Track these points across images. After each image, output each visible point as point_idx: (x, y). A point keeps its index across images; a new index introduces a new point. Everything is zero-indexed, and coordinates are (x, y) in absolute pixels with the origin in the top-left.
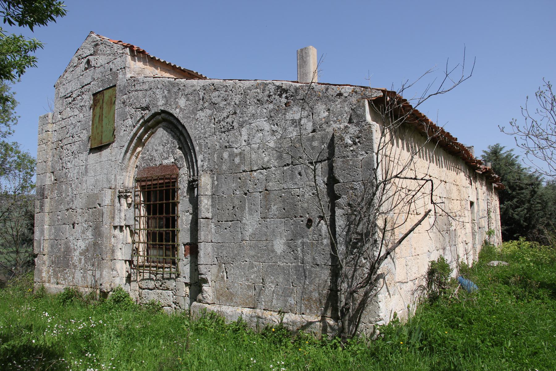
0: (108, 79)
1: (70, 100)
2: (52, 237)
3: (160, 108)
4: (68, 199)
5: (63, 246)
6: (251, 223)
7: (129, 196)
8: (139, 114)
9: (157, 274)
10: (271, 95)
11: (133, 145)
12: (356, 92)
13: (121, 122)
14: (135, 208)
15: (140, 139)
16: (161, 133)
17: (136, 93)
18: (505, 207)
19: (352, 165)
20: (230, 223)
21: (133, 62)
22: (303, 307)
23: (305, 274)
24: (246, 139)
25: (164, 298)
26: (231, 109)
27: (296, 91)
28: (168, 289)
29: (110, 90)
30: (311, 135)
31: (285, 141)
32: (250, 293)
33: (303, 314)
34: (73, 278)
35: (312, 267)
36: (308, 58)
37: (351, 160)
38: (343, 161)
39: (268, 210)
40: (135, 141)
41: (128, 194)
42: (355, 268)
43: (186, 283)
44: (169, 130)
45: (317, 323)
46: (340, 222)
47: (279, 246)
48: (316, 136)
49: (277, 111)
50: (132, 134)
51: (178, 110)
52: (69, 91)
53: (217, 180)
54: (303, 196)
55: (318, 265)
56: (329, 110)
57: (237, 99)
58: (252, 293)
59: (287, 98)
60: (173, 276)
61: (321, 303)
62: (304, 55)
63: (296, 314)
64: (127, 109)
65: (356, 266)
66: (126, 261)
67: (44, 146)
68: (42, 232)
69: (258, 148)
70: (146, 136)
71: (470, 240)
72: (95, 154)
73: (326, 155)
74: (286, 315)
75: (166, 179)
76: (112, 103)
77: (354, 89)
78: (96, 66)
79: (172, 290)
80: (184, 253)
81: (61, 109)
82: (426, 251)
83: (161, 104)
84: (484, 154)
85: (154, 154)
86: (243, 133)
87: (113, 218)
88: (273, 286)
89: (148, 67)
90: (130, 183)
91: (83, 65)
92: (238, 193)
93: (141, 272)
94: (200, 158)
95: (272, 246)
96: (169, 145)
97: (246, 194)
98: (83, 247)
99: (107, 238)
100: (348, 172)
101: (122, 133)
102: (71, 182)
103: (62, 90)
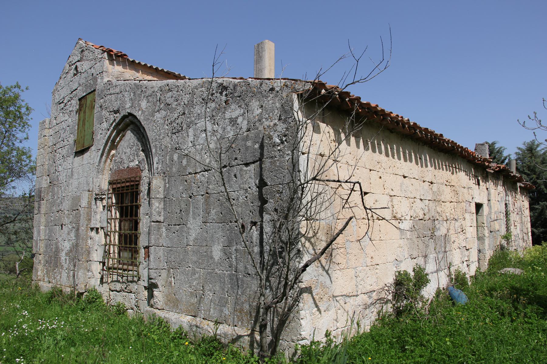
0: (90, 83)
1: (62, 105)
2: (47, 238)
3: (127, 110)
4: (59, 200)
5: (54, 246)
6: (194, 226)
7: (104, 198)
8: (112, 118)
9: (123, 276)
10: (214, 94)
11: (108, 148)
12: (287, 86)
13: (98, 125)
14: (108, 210)
15: (113, 141)
16: (129, 135)
17: (110, 96)
18: (540, 208)
19: (279, 166)
20: (178, 227)
21: (111, 66)
22: (236, 319)
23: (238, 284)
24: (192, 140)
25: (126, 300)
26: (180, 109)
27: (234, 88)
28: (131, 292)
29: (92, 94)
30: (245, 134)
31: (224, 141)
32: (192, 301)
33: (236, 326)
34: (61, 277)
35: (244, 276)
36: (264, 53)
37: (278, 160)
38: (271, 162)
39: (208, 214)
40: (109, 144)
41: (103, 197)
42: (280, 280)
43: (145, 287)
44: (135, 133)
45: (245, 337)
46: (268, 229)
47: (217, 252)
48: (250, 135)
49: (218, 109)
50: (107, 137)
51: (140, 112)
52: (62, 97)
53: (168, 183)
54: (238, 199)
55: (249, 274)
56: (262, 106)
57: (186, 99)
58: (194, 300)
59: (226, 95)
60: (136, 279)
61: (251, 315)
62: (260, 50)
63: (229, 325)
64: (104, 112)
65: (280, 278)
66: (100, 262)
67: (42, 150)
68: (39, 232)
69: (202, 149)
70: (118, 139)
71: (474, 246)
72: (79, 158)
73: (258, 155)
74: (221, 326)
75: (132, 181)
76: (93, 107)
77: (285, 83)
78: (82, 71)
79: (134, 293)
80: (144, 256)
81: (56, 114)
82: (391, 258)
83: (128, 108)
84: (518, 151)
85: (124, 157)
86: (190, 134)
87: (90, 220)
88: (211, 295)
89: (128, 70)
90: (105, 186)
91: (73, 72)
92: (184, 196)
93: (111, 274)
94: (156, 160)
95: (211, 252)
96: (134, 148)
97: (190, 197)
98: (68, 248)
99: (83, 239)
100: (275, 174)
101: (99, 137)
102: (61, 185)
103: (57, 97)
